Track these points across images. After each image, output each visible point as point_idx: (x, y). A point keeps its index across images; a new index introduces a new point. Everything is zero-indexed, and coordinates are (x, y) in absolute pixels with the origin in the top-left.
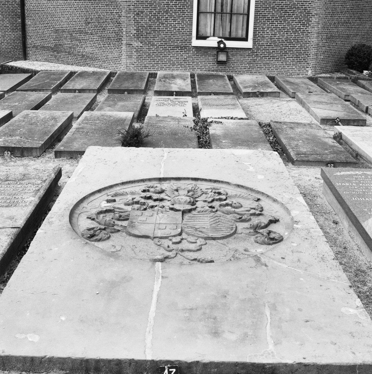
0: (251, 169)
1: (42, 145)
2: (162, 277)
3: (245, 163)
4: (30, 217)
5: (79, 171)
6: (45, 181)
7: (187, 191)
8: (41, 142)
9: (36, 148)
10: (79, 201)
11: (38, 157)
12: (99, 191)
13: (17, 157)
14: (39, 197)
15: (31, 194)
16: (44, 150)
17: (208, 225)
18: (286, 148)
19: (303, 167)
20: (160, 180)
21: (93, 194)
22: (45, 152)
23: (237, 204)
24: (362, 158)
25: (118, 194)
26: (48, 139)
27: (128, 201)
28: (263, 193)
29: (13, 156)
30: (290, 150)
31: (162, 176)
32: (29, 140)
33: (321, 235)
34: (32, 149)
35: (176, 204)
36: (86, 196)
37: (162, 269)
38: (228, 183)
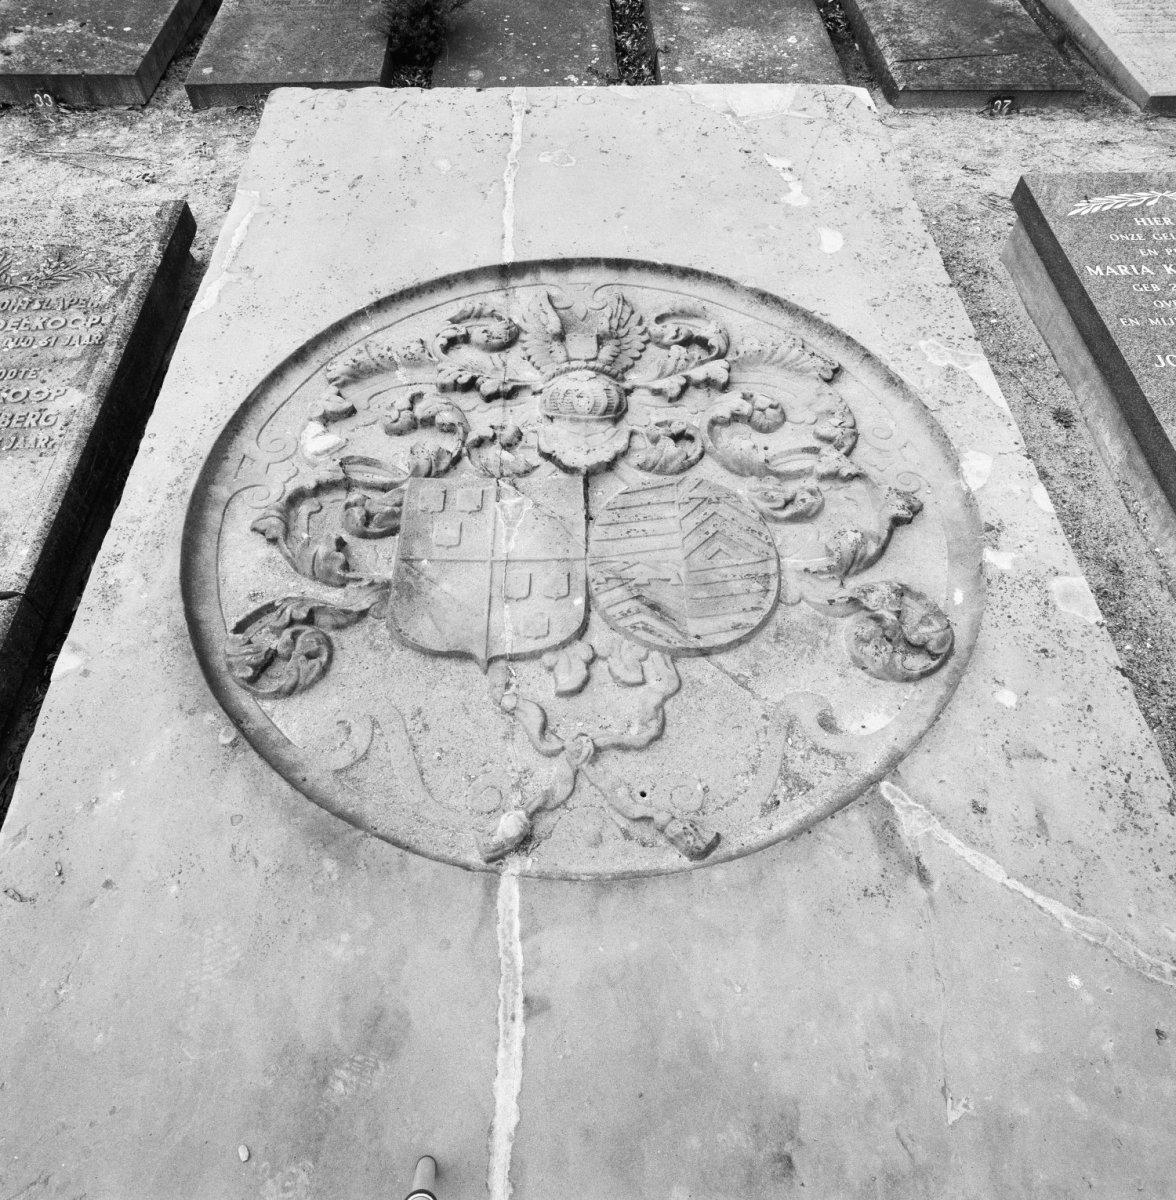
0: (796, 196)
1: (147, 60)
2: (526, 1001)
3: (771, 161)
4: (61, 514)
5: (235, 242)
6: (127, 284)
7: (594, 340)
8: (141, 45)
9: (125, 77)
10: (225, 431)
11: (144, 106)
12: (300, 356)
13: (79, 109)
14: (100, 388)
15: (71, 372)
16: (159, 75)
17: (679, 555)
18: (864, 24)
19: (921, 111)
20: (506, 272)
21: (277, 375)
22: (164, 77)
23: (770, 412)
24: (1078, 49)
25: (362, 372)
26: (167, 24)
27: (394, 414)
28: (848, 338)
29: (65, 108)
30: (882, 41)
31: (508, 258)
32: (107, 39)
33: (1092, 621)
34: (113, 78)
35: (559, 417)
36: (249, 397)
37: (523, 937)
38: (727, 283)
